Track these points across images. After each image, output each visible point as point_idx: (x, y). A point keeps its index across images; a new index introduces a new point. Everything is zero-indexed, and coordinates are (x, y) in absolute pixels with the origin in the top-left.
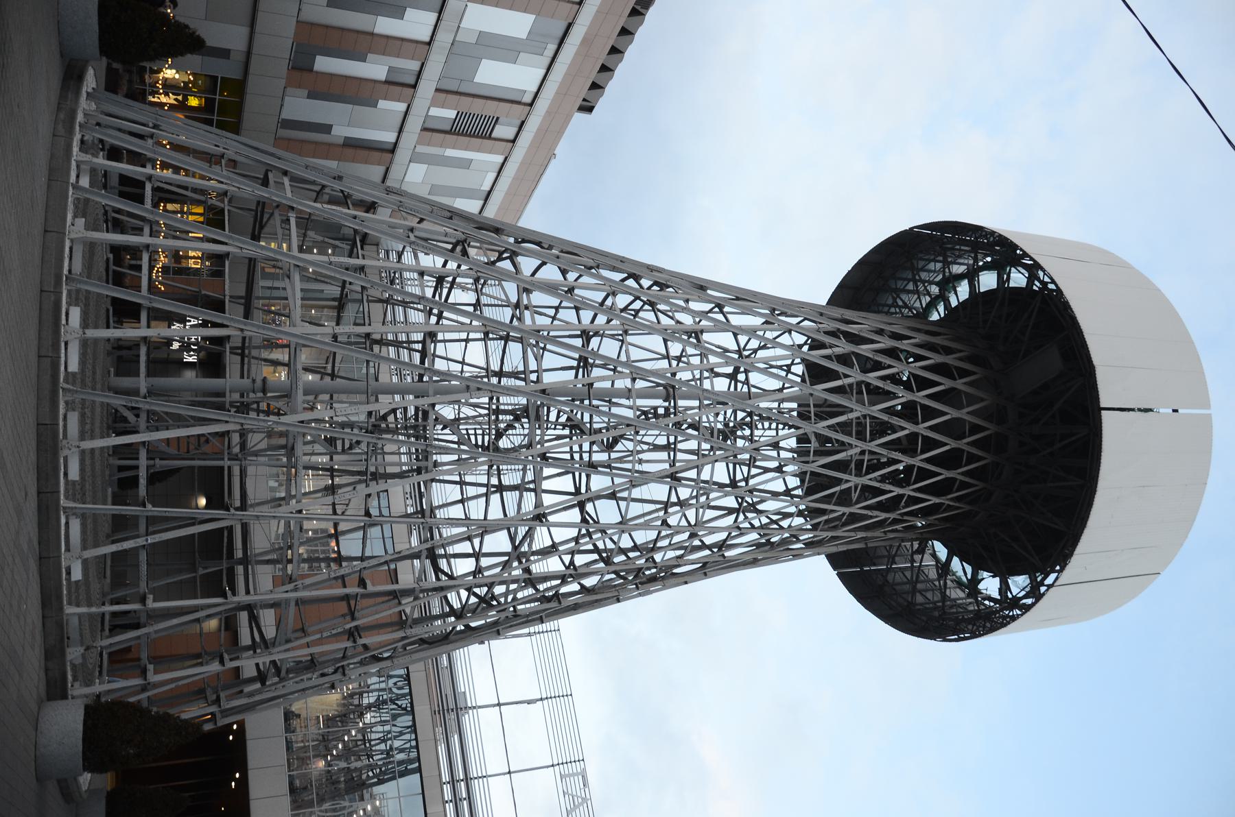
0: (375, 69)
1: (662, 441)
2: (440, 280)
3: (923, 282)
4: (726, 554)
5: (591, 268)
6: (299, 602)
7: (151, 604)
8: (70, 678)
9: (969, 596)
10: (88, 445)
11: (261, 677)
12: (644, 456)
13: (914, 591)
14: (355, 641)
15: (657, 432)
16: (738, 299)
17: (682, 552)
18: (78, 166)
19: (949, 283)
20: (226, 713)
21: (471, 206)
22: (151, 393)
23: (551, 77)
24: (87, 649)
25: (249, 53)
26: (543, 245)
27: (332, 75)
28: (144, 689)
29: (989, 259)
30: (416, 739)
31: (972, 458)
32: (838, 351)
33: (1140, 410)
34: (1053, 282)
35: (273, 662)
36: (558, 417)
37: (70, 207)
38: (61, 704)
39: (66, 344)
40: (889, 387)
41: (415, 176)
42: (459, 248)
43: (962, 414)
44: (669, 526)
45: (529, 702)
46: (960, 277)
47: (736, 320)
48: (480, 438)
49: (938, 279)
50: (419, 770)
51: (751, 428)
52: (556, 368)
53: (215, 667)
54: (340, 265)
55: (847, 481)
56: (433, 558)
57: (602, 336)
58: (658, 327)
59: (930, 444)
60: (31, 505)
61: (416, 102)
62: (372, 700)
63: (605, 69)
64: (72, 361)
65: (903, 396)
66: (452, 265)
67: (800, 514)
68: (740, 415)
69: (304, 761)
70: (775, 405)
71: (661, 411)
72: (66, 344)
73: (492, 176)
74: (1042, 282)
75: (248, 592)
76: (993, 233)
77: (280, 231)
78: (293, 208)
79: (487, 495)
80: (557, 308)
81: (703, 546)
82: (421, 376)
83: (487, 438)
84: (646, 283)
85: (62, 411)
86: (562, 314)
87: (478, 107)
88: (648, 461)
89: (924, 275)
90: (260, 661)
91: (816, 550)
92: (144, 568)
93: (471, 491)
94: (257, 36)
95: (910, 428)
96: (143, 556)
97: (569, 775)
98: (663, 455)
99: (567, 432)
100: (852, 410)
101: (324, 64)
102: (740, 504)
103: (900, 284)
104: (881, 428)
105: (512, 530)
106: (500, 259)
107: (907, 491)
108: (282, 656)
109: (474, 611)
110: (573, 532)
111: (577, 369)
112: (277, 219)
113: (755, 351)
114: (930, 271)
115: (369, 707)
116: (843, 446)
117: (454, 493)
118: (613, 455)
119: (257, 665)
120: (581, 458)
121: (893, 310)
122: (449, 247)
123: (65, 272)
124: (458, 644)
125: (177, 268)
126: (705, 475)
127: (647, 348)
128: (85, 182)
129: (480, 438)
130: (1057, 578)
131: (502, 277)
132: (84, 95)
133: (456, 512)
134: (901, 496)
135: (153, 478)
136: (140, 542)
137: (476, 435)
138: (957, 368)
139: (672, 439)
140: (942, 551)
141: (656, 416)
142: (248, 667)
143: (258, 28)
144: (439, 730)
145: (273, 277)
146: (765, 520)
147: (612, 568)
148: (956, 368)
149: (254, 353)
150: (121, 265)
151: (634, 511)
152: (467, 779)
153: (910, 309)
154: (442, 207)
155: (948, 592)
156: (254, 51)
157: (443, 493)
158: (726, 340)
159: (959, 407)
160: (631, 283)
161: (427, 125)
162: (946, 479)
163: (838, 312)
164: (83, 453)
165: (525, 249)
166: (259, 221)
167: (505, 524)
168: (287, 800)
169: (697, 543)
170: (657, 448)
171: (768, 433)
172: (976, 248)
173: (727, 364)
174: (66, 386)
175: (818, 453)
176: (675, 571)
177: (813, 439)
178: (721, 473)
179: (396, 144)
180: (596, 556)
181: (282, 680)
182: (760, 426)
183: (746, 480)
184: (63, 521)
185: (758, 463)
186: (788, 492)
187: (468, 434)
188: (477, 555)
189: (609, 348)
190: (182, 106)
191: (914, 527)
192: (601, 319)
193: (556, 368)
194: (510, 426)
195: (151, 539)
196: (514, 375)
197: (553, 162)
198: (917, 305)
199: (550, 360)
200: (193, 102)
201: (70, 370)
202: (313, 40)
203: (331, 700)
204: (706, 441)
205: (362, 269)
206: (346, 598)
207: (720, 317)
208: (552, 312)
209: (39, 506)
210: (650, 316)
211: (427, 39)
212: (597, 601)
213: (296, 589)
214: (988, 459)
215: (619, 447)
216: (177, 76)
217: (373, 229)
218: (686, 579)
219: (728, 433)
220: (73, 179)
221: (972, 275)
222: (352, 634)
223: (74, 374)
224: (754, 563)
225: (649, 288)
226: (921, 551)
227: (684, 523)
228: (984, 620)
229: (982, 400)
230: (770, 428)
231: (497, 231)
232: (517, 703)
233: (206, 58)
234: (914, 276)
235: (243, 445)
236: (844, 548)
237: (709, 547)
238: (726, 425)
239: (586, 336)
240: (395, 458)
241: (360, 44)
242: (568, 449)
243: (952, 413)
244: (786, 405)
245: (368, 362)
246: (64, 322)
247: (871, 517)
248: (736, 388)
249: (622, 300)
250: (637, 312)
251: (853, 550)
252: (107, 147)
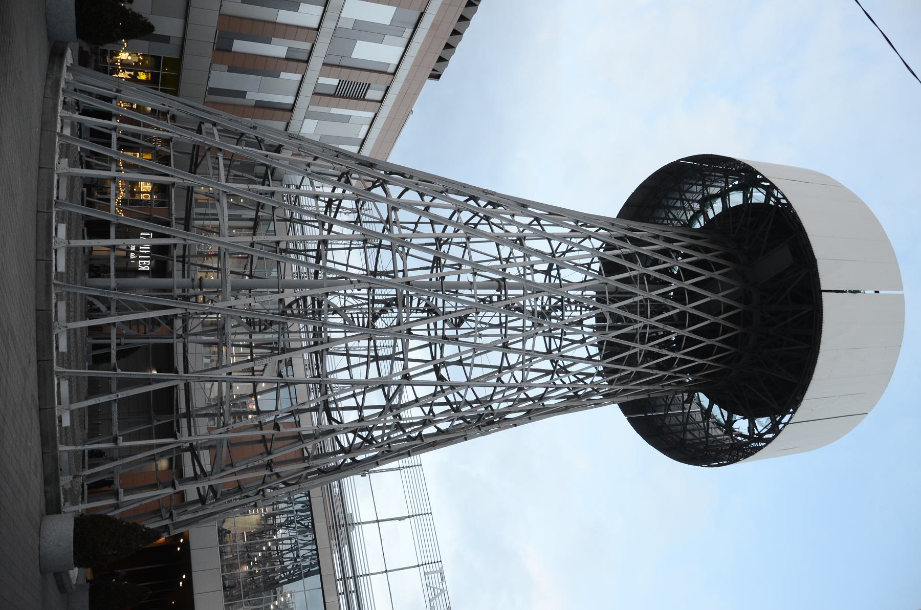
0: (277, 49)
1: (496, 321)
2: (329, 204)
3: (688, 200)
4: (545, 403)
5: (442, 192)
6: (231, 444)
7: (121, 443)
8: (62, 500)
9: (726, 433)
10: (72, 325)
11: (202, 500)
12: (483, 332)
13: (685, 430)
14: (271, 471)
15: (492, 314)
16: (550, 214)
17: (511, 403)
18: (62, 121)
19: (707, 201)
20: (178, 525)
21: (354, 149)
22: (120, 288)
23: (408, 53)
24: (75, 477)
25: (184, 39)
26: (407, 176)
27: (245, 54)
28: (116, 507)
29: (736, 183)
30: (317, 549)
31: (726, 330)
32: (625, 251)
33: (850, 291)
34: (784, 198)
35: (211, 487)
36: (419, 304)
37: (57, 150)
38: (57, 516)
39: (56, 251)
40: (665, 278)
41: (309, 128)
42: (343, 180)
43: (719, 297)
44: (502, 382)
45: (400, 519)
46: (716, 196)
47: (549, 230)
48: (361, 320)
49: (698, 198)
51: (562, 310)
52: (417, 264)
53: (169, 491)
54: (256, 191)
55: (634, 348)
56: (328, 411)
57: (450, 244)
58: (493, 235)
59: (695, 319)
60: (33, 370)
61: (309, 73)
62: (283, 521)
63: (441, 60)
65: (675, 284)
66: (339, 191)
67: (599, 374)
68: (554, 301)
70: (580, 293)
71: (495, 299)
72: (56, 251)
73: (366, 128)
74: (776, 198)
75: (190, 435)
76: (739, 162)
77: (211, 171)
78: (220, 150)
79: (367, 363)
80: (416, 224)
81: (528, 399)
82: (316, 273)
83: (366, 320)
84: (482, 203)
85: (54, 301)
86: (420, 228)
87: (354, 77)
88: (486, 336)
89: (688, 196)
90: (200, 486)
91: (613, 399)
92: (115, 416)
93: (354, 361)
94: (189, 27)
95: (680, 308)
96: (115, 408)
97: (431, 573)
98: (497, 331)
99: (425, 315)
100: (636, 295)
101: (240, 46)
102: (555, 367)
103: (671, 203)
104: (659, 308)
105: (386, 389)
106: (374, 186)
107: (679, 355)
108: (217, 482)
109: (360, 448)
110: (432, 390)
111: (432, 268)
112: (209, 161)
113: (564, 253)
114: (692, 192)
115: (281, 526)
116: (630, 322)
117: (342, 362)
118: (460, 332)
119: (198, 489)
120: (436, 333)
121: (665, 222)
122: (336, 179)
124: (348, 472)
125: (132, 201)
126: (529, 346)
127: (484, 250)
128: (67, 132)
129: (361, 320)
130: (791, 418)
131: (376, 199)
132: (65, 68)
133: (345, 375)
134: (674, 359)
135: (121, 354)
136: (113, 397)
137: (358, 318)
138: (715, 263)
139: (503, 320)
140: (705, 401)
141: (491, 302)
142: (191, 492)
144: (333, 542)
145: (205, 205)
146: (573, 379)
147: (460, 415)
148: (713, 263)
149: (193, 260)
150: (95, 191)
151: (475, 370)
152: (355, 577)
153: (679, 221)
154: (330, 149)
155: (710, 431)
156: (188, 37)
157: (334, 362)
158: (543, 246)
159: (716, 292)
160: (472, 202)
161: (317, 91)
162: (707, 345)
163: (626, 223)
165: (393, 179)
166: (195, 159)
167: (381, 385)
168: (221, 594)
169: (523, 396)
170: (492, 326)
171: (575, 314)
172: (726, 174)
173: (543, 262)
174: (56, 282)
175: (612, 328)
176: (508, 416)
177: (608, 318)
178: (540, 344)
179: (294, 105)
180: (448, 407)
181: (217, 500)
182: (568, 309)
183: (559, 349)
184: (56, 382)
185: (567, 337)
186: (590, 358)
187: (352, 317)
188: (360, 408)
189: (456, 251)
190: (134, 79)
191: (683, 382)
192: (450, 230)
193: (417, 264)
194: (383, 311)
195: (122, 395)
196: (386, 273)
197: (411, 116)
198: (684, 217)
199: (412, 263)
200: (142, 76)
201: (59, 270)
202: (231, 28)
203: (253, 518)
204: (529, 318)
205: (273, 194)
206: (264, 440)
207: (539, 228)
208: (412, 226)
209: (39, 371)
210: (486, 228)
211: (316, 26)
212: (450, 439)
213: (227, 432)
214: (739, 330)
215: (465, 325)
216: (130, 58)
217: (280, 164)
218: (515, 423)
219: (544, 314)
220: (59, 130)
221: (724, 195)
222: (269, 466)
223: (61, 273)
224: (565, 410)
225: (485, 206)
226: (690, 401)
227: (513, 381)
228: (736, 451)
229: (733, 286)
230: (576, 310)
231: (371, 165)
232: (391, 520)
233: (152, 43)
234: (681, 196)
235: (185, 329)
236: (632, 398)
237: (532, 399)
238: (543, 308)
239: (439, 242)
240: (296, 336)
241: (268, 31)
242: (425, 326)
243: (711, 297)
244: (587, 293)
245: (278, 262)
246: (54, 235)
247: (652, 375)
248: (550, 281)
249: (465, 216)
250: (476, 225)
251: (639, 400)
252: (81, 108)
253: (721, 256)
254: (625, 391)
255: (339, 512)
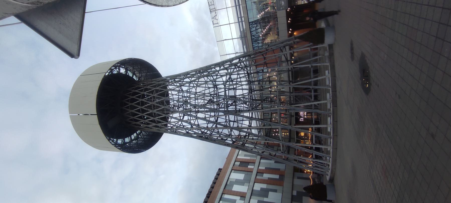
0: (266, 176)
7: (310, 65)
10: (325, 102)
25: (293, 178)
31: (128, 101)
34: (110, 142)
45: (226, 40)
46: (134, 140)
50: (249, 23)
54: (271, 141)
59: (138, 104)
60: (338, 89)
64: (330, 120)
69: (274, 24)
78: (284, 159)
85: (331, 109)
87: (243, 169)
95: (143, 107)
101: (277, 177)
123: (332, 140)
128: (328, 158)
140: (134, 77)
143: (291, 184)
151: (203, 88)
152: (239, 22)
159: (131, 112)
163: (161, 132)
164: (326, 100)
168: (278, 16)
195: (310, 80)
220: (331, 159)
221: (132, 140)
235: (290, 98)
236: (157, 79)
241: (269, 181)
243: (133, 111)
253: (131, 123)
254: (159, 81)
255: (244, 41)
